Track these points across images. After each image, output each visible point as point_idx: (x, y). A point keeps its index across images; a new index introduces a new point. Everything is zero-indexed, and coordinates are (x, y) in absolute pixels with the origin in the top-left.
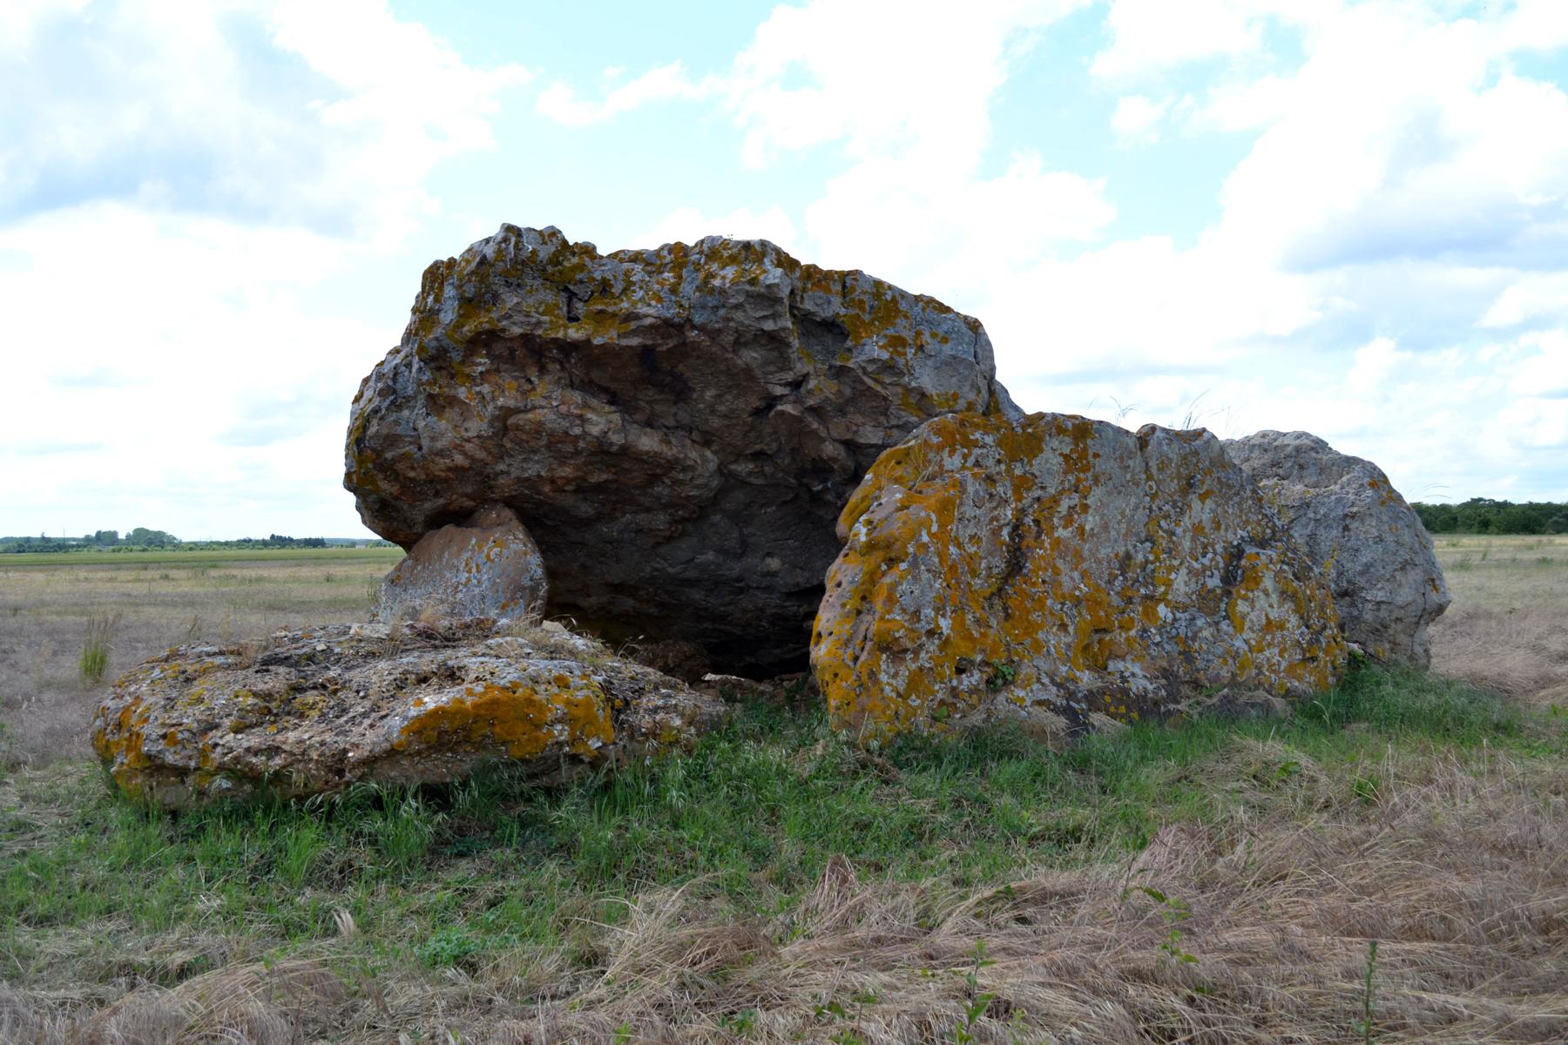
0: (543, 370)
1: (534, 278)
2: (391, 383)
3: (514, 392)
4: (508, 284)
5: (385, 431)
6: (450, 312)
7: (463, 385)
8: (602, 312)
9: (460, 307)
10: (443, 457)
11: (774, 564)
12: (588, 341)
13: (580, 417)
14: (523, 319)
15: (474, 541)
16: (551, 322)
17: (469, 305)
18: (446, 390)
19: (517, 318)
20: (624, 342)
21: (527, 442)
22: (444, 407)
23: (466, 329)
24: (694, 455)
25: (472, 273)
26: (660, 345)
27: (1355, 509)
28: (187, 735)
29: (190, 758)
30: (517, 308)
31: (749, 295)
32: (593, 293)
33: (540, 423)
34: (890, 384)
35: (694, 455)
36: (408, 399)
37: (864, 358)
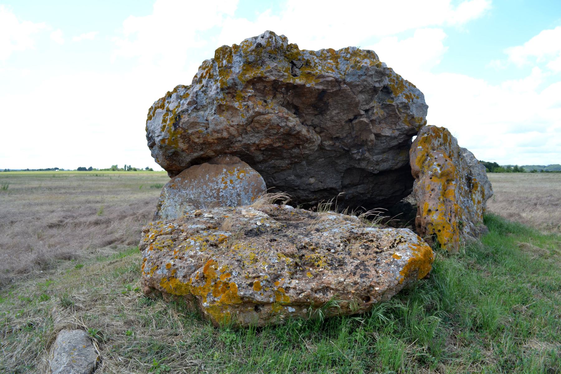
0: (274, 97)
1: (281, 56)
2: (195, 99)
3: (261, 106)
4: (270, 57)
5: (192, 120)
6: (237, 68)
7: (239, 101)
8: (309, 73)
9: (244, 66)
10: (218, 133)
11: (312, 180)
12: (304, 85)
13: (287, 118)
14: (277, 73)
15: (225, 170)
16: (288, 75)
17: (249, 65)
18: (228, 103)
19: (274, 72)
20: (317, 87)
21: (258, 128)
22: (224, 111)
23: (247, 76)
24: (315, 137)
25: (253, 51)
26: (329, 90)
27: (471, 165)
28: (265, 282)
29: (270, 297)
30: (275, 68)
31: (376, 72)
32: (303, 65)
33: (270, 120)
34: (403, 113)
35: (315, 137)
36: (203, 106)
37: (399, 101)
